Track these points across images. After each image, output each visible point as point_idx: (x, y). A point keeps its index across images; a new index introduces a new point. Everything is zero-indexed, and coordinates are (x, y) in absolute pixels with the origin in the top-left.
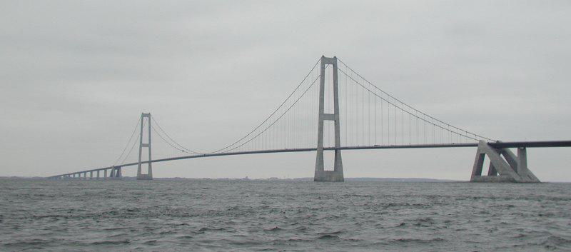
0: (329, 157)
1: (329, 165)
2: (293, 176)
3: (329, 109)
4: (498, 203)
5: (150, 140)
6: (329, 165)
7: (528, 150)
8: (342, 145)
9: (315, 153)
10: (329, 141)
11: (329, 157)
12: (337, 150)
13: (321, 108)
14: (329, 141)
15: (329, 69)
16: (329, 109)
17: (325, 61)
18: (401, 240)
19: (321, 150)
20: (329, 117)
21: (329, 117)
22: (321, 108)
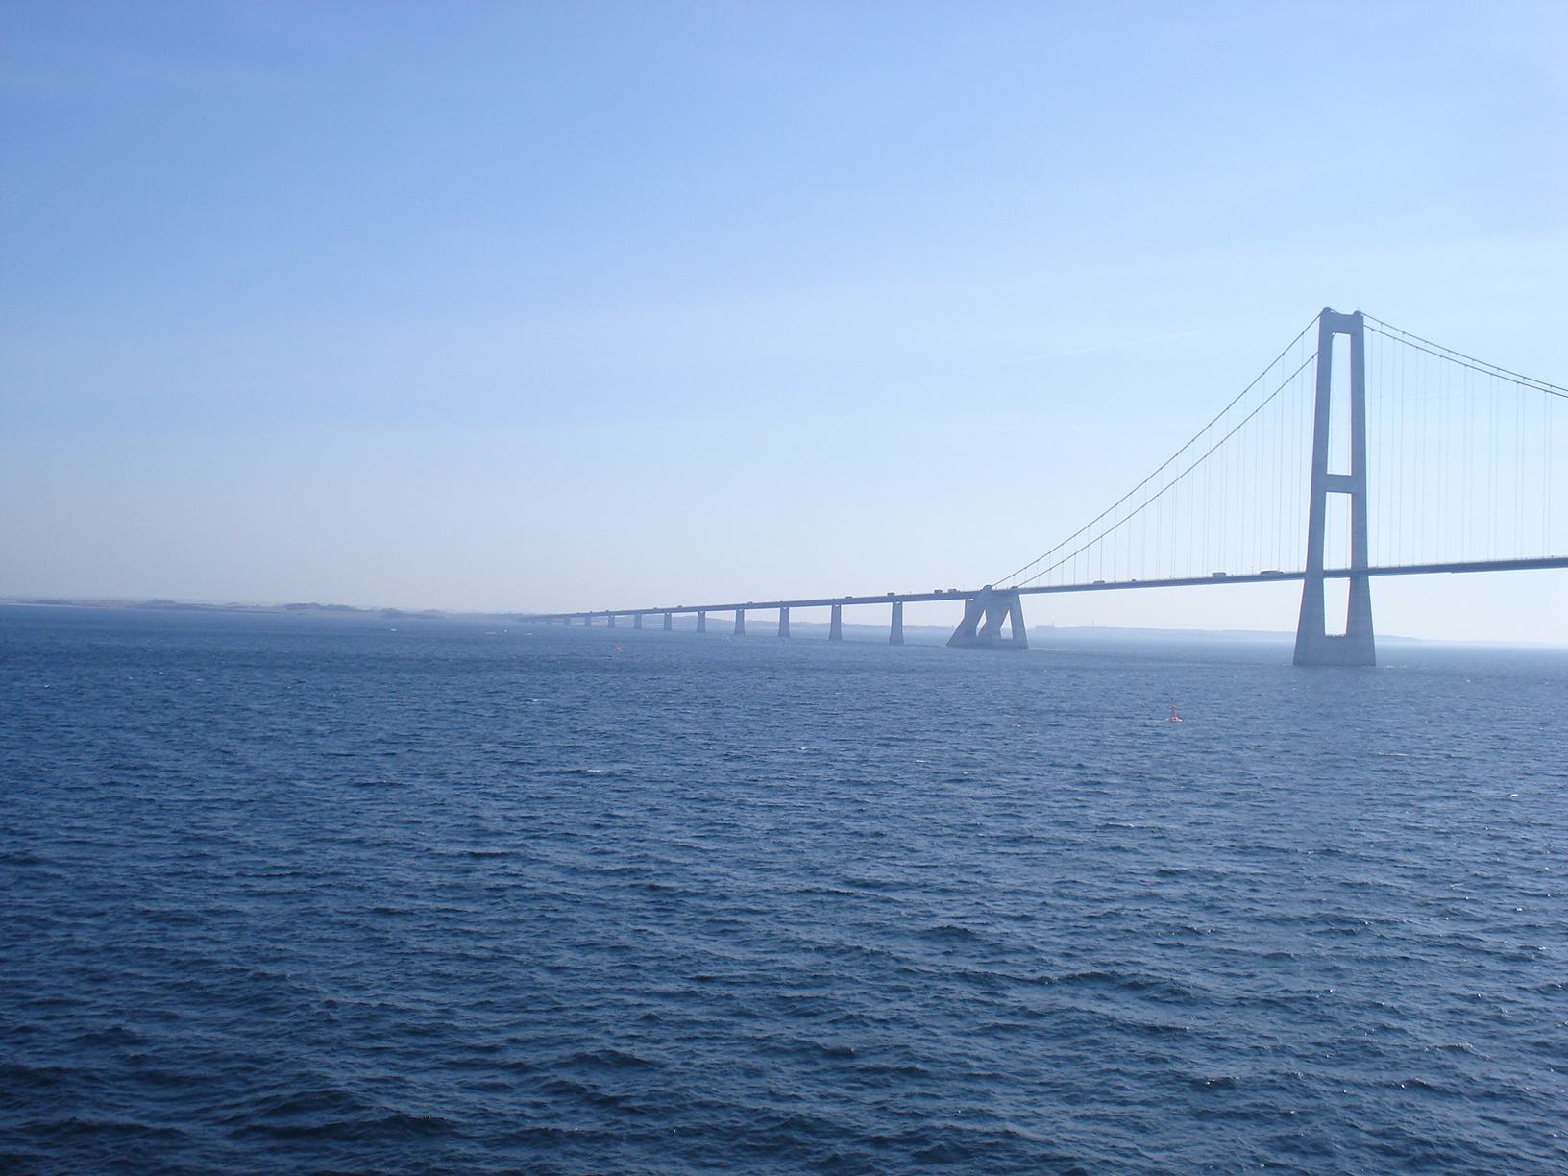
0: (1336, 595)
1: (1336, 622)
2: (817, 621)
3: (1339, 463)
4: (1397, 952)
5: (938, 596)
6: (1336, 622)
7: (791, 610)
8: (1372, 563)
9: (1299, 585)
10: (1337, 553)
11: (1336, 595)
12: (1359, 574)
13: (751, 606)
14: (1337, 553)
15: (1341, 343)
16: (1339, 463)
17: (1331, 323)
18: (1529, 926)
19: (1314, 576)
20: (1339, 484)
21: (1339, 484)
22: (751, 606)
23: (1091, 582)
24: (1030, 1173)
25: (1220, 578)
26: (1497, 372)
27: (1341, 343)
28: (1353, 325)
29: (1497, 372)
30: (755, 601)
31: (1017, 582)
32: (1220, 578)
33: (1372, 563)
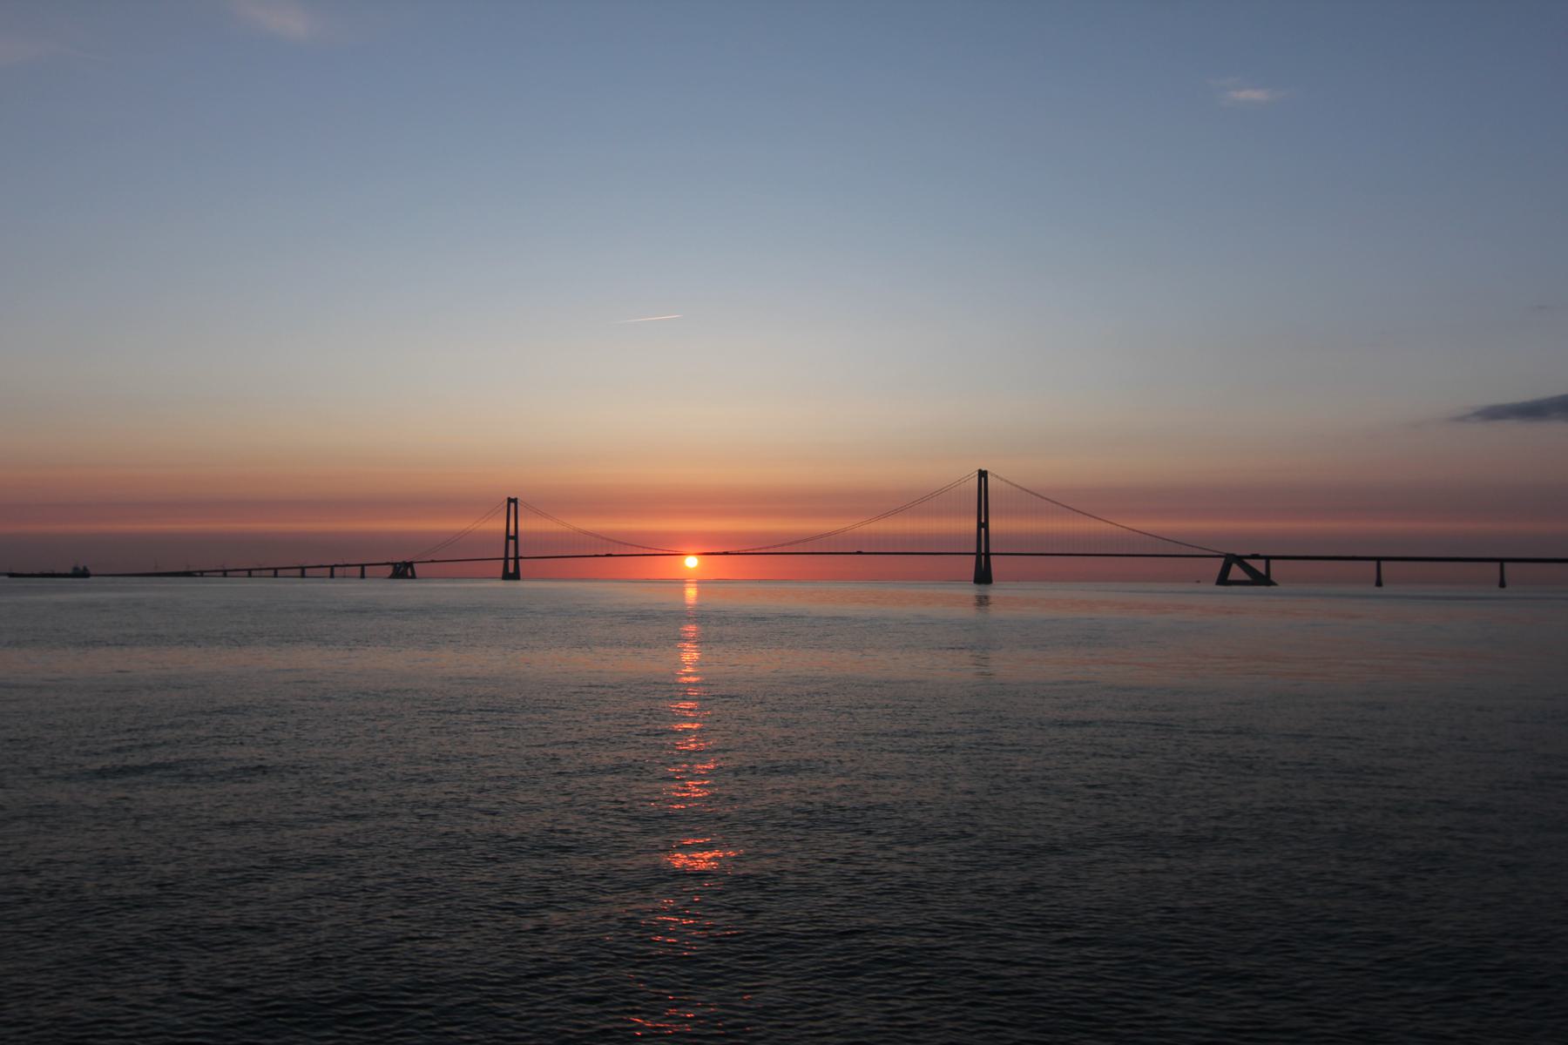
0: (511, 563)
9: (502, 561)
10: (512, 554)
11: (511, 563)
12: (517, 559)
14: (512, 554)
15: (512, 505)
17: (510, 500)
19: (506, 559)
20: (512, 538)
23: (384, 562)
24: (515, 1043)
25: (433, 561)
26: (1079, 512)
27: (512, 505)
28: (515, 501)
29: (1079, 512)
30: (56, 572)
31: (415, 560)
32: (433, 561)
33: (991, 552)
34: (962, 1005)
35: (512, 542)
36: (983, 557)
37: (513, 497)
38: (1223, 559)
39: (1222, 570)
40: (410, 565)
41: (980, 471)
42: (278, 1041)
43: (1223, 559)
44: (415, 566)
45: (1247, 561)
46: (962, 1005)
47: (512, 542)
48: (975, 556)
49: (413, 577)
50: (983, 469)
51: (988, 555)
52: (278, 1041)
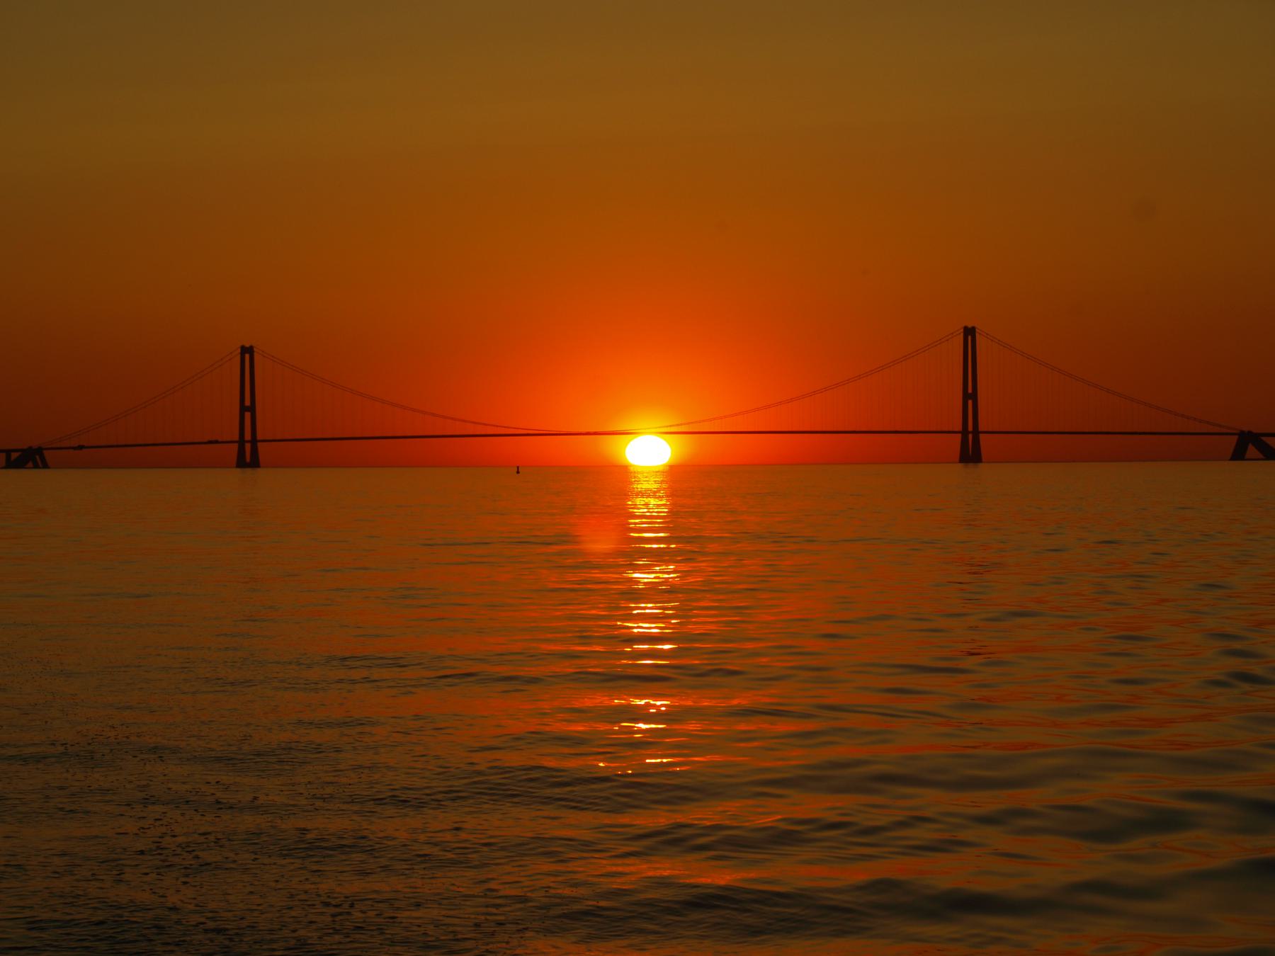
0: (248, 446)
9: (236, 445)
10: (248, 436)
11: (248, 446)
14: (248, 436)
32: (81, 447)
33: (258, 438)
34: (424, 794)
35: (248, 415)
36: (970, 436)
37: (247, 345)
38: (1237, 437)
39: (980, 454)
40: (40, 451)
41: (966, 328)
42: (592, 954)
43: (1237, 437)
44: (45, 452)
45: (1264, 438)
46: (424, 794)
47: (248, 415)
48: (960, 435)
49: (46, 466)
50: (970, 326)
51: (976, 432)
52: (592, 954)
